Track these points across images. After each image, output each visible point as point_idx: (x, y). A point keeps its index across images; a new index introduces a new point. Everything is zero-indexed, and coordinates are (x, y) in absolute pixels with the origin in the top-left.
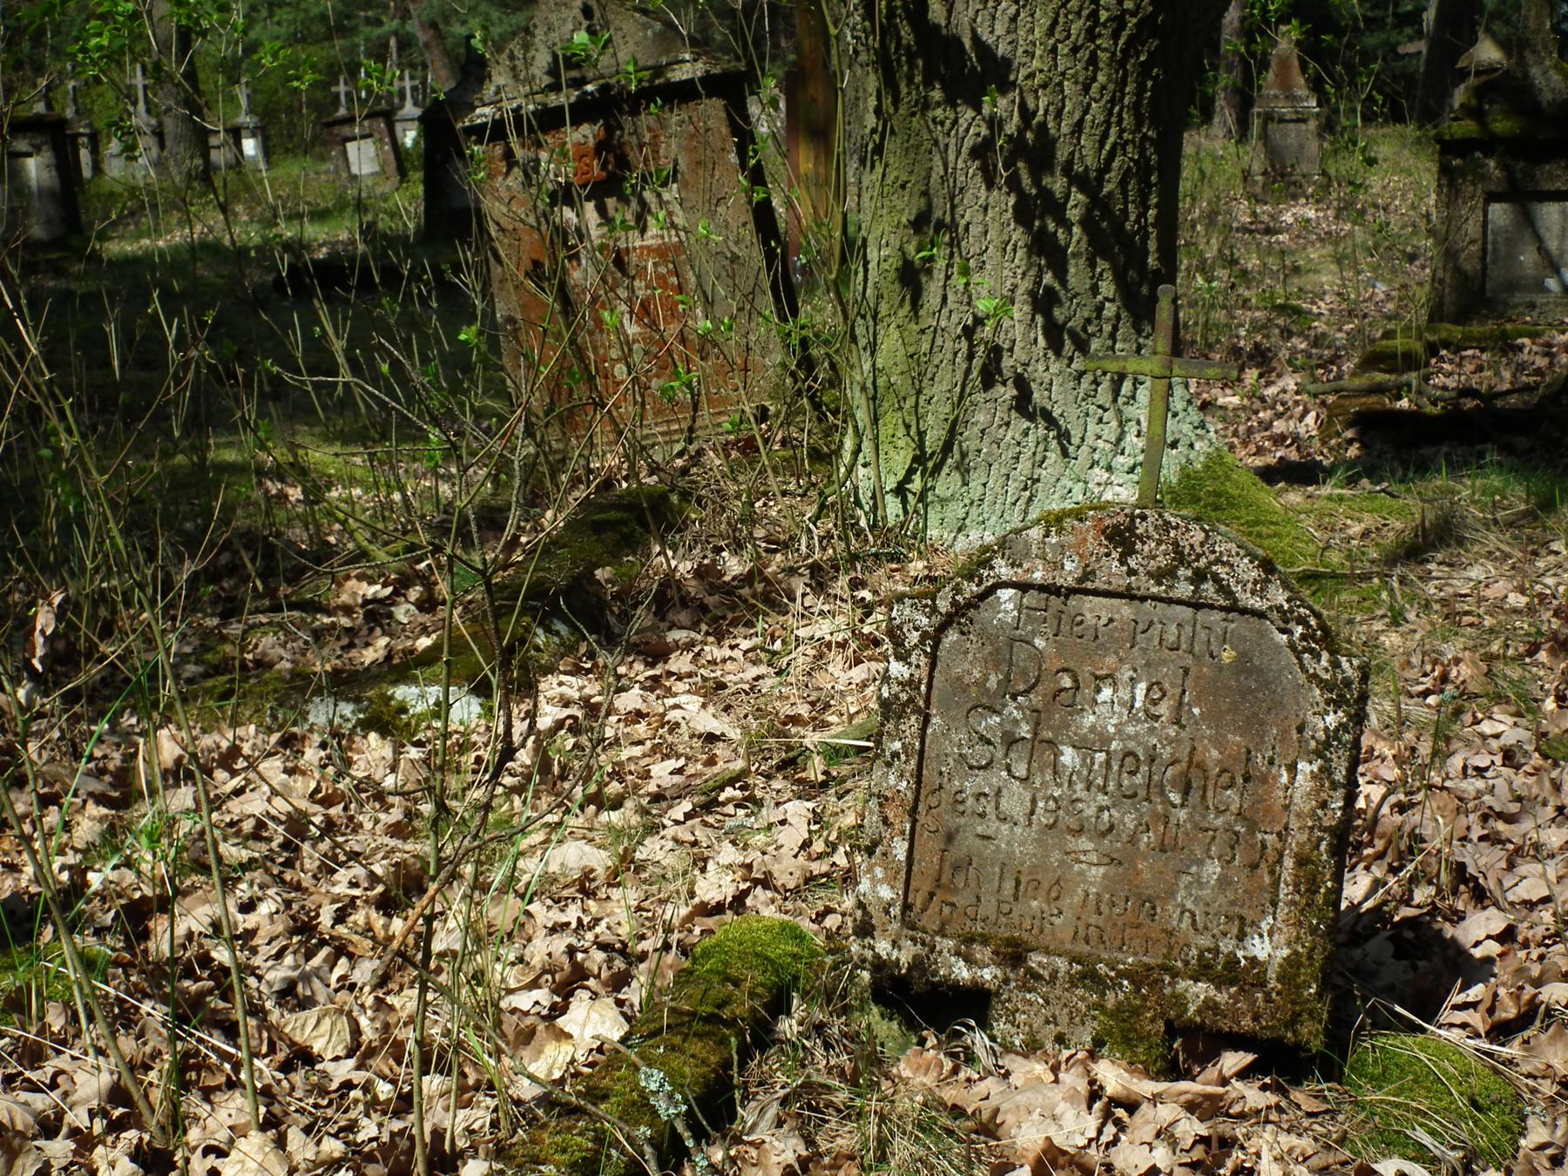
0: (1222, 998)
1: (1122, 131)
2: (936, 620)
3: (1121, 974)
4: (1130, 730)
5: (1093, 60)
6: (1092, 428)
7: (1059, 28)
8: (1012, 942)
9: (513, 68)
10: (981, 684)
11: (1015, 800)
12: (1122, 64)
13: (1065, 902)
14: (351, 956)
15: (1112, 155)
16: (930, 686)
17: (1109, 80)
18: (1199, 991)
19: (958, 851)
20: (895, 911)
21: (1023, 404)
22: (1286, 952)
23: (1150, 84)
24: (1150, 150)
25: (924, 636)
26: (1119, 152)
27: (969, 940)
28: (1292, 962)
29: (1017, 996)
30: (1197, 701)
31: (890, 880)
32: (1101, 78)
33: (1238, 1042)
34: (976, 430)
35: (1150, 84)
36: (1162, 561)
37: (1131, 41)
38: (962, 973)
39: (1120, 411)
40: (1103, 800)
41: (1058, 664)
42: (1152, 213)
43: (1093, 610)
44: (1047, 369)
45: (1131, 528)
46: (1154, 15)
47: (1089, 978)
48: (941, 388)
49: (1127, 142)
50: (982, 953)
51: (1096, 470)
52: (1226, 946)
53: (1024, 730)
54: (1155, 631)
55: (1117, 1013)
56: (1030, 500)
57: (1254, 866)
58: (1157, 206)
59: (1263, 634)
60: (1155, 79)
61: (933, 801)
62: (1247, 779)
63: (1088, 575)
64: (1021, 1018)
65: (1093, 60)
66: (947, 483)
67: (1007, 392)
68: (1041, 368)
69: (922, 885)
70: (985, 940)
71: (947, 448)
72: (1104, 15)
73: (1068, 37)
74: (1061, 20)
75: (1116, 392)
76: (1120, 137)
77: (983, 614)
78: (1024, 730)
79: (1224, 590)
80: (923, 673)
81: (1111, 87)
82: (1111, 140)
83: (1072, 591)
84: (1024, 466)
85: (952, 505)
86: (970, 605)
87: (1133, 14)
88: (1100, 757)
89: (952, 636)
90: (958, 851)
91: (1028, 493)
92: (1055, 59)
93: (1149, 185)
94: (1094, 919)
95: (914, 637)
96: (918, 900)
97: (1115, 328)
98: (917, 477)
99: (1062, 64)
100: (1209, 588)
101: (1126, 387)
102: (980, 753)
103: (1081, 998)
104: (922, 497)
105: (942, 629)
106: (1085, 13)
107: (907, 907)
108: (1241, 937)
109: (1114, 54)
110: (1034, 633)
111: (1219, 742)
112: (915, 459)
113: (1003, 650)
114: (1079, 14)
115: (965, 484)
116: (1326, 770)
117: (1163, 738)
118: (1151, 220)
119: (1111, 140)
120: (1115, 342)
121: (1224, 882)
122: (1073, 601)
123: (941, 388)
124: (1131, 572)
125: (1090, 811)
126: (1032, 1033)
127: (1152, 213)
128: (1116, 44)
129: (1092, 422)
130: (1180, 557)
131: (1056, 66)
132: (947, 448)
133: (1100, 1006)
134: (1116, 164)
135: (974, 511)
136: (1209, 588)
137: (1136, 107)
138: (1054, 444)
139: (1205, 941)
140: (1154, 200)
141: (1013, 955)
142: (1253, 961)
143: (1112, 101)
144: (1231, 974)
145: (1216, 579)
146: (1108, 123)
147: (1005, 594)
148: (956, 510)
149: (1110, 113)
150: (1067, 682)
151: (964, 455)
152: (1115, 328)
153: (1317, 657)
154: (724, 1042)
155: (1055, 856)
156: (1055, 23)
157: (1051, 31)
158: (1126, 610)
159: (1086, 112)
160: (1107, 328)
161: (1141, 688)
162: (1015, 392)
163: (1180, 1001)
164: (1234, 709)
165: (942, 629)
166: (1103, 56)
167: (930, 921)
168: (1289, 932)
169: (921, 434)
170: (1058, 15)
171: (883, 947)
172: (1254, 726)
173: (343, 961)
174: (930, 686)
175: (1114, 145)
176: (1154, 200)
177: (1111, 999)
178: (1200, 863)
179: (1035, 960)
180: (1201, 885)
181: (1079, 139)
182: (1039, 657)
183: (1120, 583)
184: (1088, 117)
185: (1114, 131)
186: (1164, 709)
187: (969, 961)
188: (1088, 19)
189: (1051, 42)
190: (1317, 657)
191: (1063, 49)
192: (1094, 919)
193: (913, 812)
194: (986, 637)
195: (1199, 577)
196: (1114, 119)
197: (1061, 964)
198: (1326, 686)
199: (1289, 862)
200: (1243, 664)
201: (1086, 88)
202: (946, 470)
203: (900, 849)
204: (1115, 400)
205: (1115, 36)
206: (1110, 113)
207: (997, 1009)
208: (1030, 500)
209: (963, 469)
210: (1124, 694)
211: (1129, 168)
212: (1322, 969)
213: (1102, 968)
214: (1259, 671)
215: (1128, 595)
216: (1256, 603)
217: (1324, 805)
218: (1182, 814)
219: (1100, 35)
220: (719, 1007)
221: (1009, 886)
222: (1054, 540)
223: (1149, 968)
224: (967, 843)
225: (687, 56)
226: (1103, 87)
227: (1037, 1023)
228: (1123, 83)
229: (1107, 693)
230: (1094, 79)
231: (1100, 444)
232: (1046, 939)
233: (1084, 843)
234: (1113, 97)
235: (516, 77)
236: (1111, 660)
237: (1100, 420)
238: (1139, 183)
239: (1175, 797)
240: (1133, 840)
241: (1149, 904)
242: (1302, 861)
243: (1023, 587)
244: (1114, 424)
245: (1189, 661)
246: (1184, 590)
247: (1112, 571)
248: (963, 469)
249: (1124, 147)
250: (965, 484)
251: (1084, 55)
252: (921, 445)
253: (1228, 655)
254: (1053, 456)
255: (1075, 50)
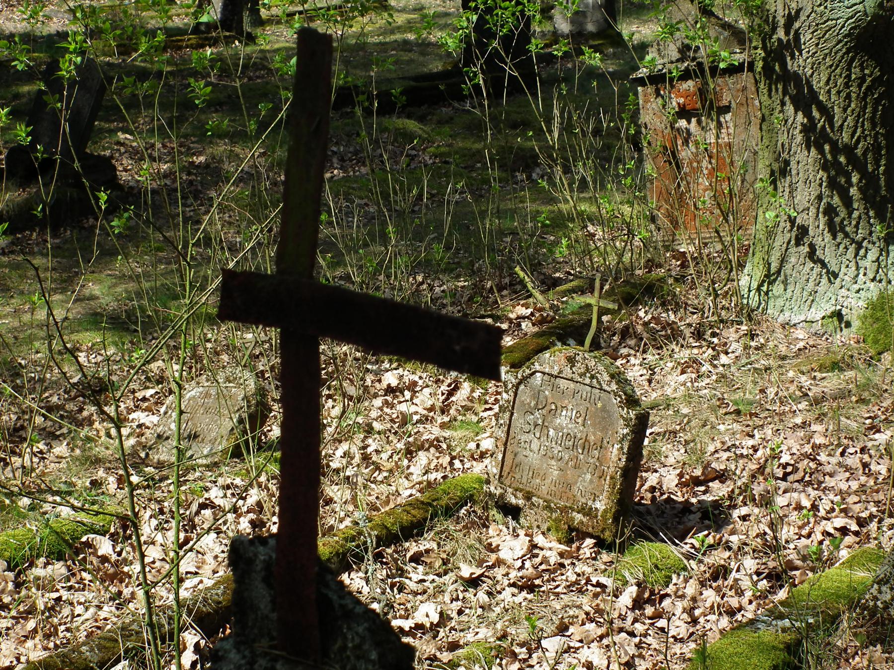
0: (585, 520)
1: (864, 130)
2: (517, 381)
3: (558, 508)
4: (570, 426)
5: (848, 97)
6: (843, 269)
7: (831, 82)
8: (528, 492)
9: (659, 50)
10: (529, 404)
11: (535, 445)
12: (864, 98)
13: (546, 481)
14: (380, 470)
15: (858, 141)
16: (514, 403)
17: (857, 107)
18: (578, 517)
19: (517, 460)
20: (497, 477)
21: (812, 254)
22: (604, 507)
23: (880, 108)
24: (881, 139)
25: (513, 386)
26: (862, 140)
27: (516, 490)
28: (605, 511)
29: (528, 510)
30: (590, 419)
31: (496, 467)
32: (853, 105)
33: (591, 536)
34: (791, 265)
35: (880, 108)
36: (583, 370)
37: (868, 88)
38: (513, 501)
39: (857, 263)
40: (560, 448)
41: (551, 401)
42: (882, 168)
43: (563, 384)
44: (823, 240)
45: (575, 358)
46: (882, 76)
47: (548, 508)
48: (780, 241)
49: (867, 135)
50: (520, 495)
51: (843, 290)
52: (590, 503)
53: (540, 422)
54: (580, 394)
55: (555, 520)
56: (813, 301)
57: (601, 477)
58: (885, 165)
59: (610, 399)
60: (884, 105)
61: (512, 441)
62: (601, 447)
63: (561, 372)
64: (528, 518)
65: (848, 97)
66: (778, 288)
67: (805, 249)
68: (820, 239)
69: (506, 469)
70: (521, 491)
71: (779, 272)
72: (853, 76)
73: (836, 86)
74: (832, 78)
75: (856, 255)
76: (863, 132)
77: (531, 380)
78: (540, 422)
79: (599, 382)
80: (512, 399)
81: (858, 110)
82: (858, 134)
83: (556, 377)
84: (811, 284)
85: (779, 300)
86: (527, 377)
87: (870, 76)
88: (561, 434)
89: (522, 387)
90: (517, 460)
91: (811, 298)
92: (830, 96)
93: (881, 156)
94: (553, 488)
95: (510, 386)
96: (505, 474)
97: (858, 223)
98: (766, 284)
99: (833, 98)
100: (595, 381)
101: (862, 252)
102: (527, 428)
103: (546, 514)
104: (767, 293)
105: (519, 384)
106: (844, 75)
107: (501, 476)
108: (594, 500)
109: (859, 95)
110: (546, 389)
111: (595, 435)
112: (766, 276)
113: (537, 395)
114: (840, 75)
115: (785, 290)
116: (622, 448)
117: (578, 430)
118: (881, 172)
119: (858, 134)
120: (858, 229)
121: (591, 481)
122: (558, 380)
123: (780, 241)
124: (573, 373)
125: (556, 452)
126: (531, 524)
127: (882, 168)
128: (860, 90)
129: (843, 266)
130: (587, 369)
131: (830, 99)
132: (779, 272)
133: (551, 518)
134: (860, 146)
135: (788, 303)
136: (595, 381)
137: (872, 120)
138: (824, 276)
139: (584, 500)
140: (883, 162)
141: (528, 497)
142: (596, 509)
143: (859, 116)
144: (588, 512)
145: (597, 379)
146: (856, 127)
147: (538, 375)
148: (780, 302)
149: (857, 122)
150: (553, 407)
151: (786, 276)
152: (858, 223)
153: (623, 409)
154: (427, 511)
155: (545, 465)
156: (829, 79)
157: (827, 83)
158: (572, 385)
159: (845, 121)
160: (854, 223)
161: (574, 412)
162: (808, 250)
163: (573, 519)
164: (600, 423)
165: (519, 384)
166: (854, 95)
167: (507, 482)
168: (606, 501)
169: (769, 264)
170: (830, 76)
171: (492, 488)
172: (604, 430)
173: (377, 472)
174: (514, 403)
175: (859, 137)
176: (883, 162)
177: (554, 515)
178: (585, 474)
179: (534, 499)
180: (585, 482)
181: (841, 133)
182: (546, 398)
183: (570, 376)
184: (846, 124)
185: (859, 130)
186: (580, 420)
187: (516, 497)
188: (845, 78)
189: (828, 88)
190: (623, 409)
191: (833, 91)
192: (553, 488)
193: (505, 444)
194: (532, 389)
195: (592, 377)
196: (859, 125)
197: (541, 501)
198: (625, 420)
199: (608, 478)
200: (604, 409)
201: (845, 110)
202: (777, 282)
203: (500, 456)
204: (855, 257)
205: (860, 86)
206: (857, 122)
207: (522, 515)
208: (813, 301)
209: (785, 283)
210: (569, 414)
211: (868, 147)
212: (614, 514)
213: (552, 505)
214: (608, 411)
215: (571, 380)
216: (607, 388)
217: (620, 459)
218: (582, 457)
219: (852, 86)
220: (433, 501)
221: (531, 473)
222: (552, 358)
223: (566, 507)
224: (520, 457)
225: (738, 51)
226: (853, 110)
227: (533, 520)
228: (865, 107)
229: (564, 413)
230: (849, 106)
231: (846, 278)
232: (539, 493)
233: (553, 462)
234: (859, 114)
235: (660, 54)
236: (566, 401)
237: (847, 266)
238: (874, 154)
239: (580, 451)
240: (567, 463)
241: (570, 486)
242: (612, 478)
243: (544, 373)
244: (854, 268)
245: (589, 405)
246: (588, 381)
247: (567, 373)
248: (785, 283)
249: (865, 138)
250: (785, 290)
251: (843, 95)
252: (769, 270)
253: (599, 405)
254: (824, 280)
255: (839, 92)
